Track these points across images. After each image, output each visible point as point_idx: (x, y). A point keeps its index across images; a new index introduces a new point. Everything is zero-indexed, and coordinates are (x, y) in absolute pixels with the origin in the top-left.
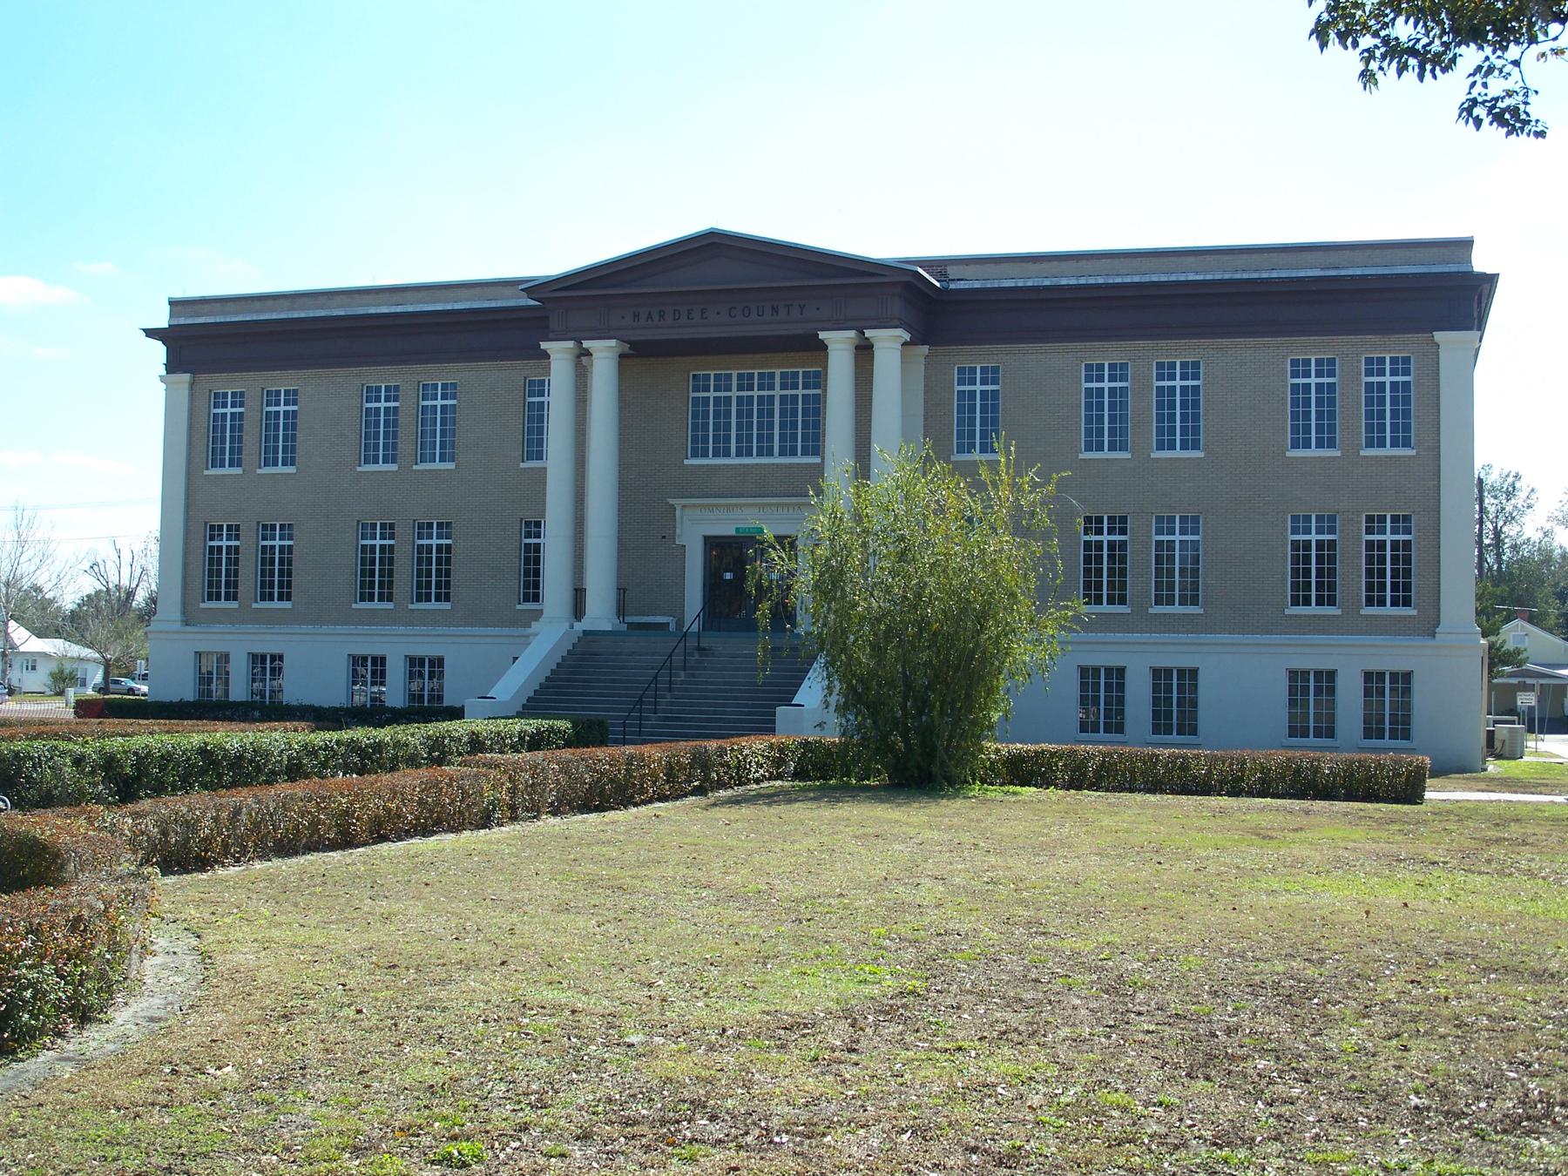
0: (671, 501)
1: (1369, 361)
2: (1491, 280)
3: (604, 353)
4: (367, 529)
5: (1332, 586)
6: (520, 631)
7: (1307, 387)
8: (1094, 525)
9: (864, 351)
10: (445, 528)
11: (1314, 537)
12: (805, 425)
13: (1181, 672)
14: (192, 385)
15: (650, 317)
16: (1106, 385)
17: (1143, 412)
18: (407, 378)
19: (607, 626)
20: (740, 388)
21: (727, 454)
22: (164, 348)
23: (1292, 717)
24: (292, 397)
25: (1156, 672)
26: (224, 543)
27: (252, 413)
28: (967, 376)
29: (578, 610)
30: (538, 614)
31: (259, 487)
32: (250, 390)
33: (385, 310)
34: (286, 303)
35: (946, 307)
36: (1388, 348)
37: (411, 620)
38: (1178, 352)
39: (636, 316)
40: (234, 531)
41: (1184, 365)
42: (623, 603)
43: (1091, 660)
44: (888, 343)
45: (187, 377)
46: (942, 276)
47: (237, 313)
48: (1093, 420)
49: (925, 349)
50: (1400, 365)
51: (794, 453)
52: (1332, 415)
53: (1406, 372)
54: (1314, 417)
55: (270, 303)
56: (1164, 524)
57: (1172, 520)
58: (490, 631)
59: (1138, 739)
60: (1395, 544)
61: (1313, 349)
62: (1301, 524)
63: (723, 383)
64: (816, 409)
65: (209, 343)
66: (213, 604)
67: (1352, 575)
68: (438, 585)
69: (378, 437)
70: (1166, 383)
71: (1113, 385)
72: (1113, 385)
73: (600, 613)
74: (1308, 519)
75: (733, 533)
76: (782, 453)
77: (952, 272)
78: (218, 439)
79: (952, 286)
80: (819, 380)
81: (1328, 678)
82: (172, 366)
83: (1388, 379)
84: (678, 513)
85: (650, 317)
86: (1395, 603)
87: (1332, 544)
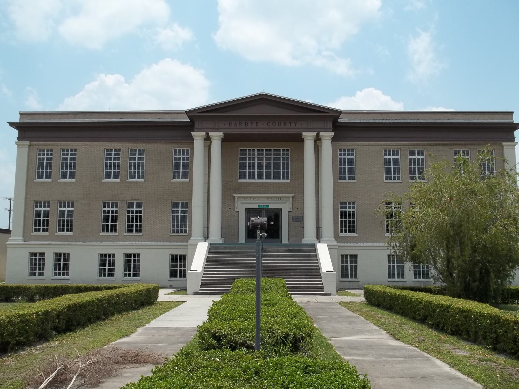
0: (234, 195)
3: (216, 138)
4: (106, 204)
6: (184, 244)
7: (345, 159)
8: (106, 204)
10: (71, 204)
12: (345, 169)
14: (29, 146)
15: (236, 125)
16: (392, 157)
17: (404, 167)
21: (253, 178)
24: (73, 152)
26: (110, 209)
30: (190, 236)
31: (57, 187)
32: (58, 150)
34: (73, 116)
35: (347, 129)
37: (58, 238)
38: (70, 146)
39: (230, 124)
43: (59, 251)
44: (327, 137)
45: (28, 143)
52: (398, 169)
58: (159, 243)
59: (49, 277)
60: (137, 212)
65: (33, 130)
66: (37, 233)
67: (122, 222)
68: (112, 226)
70: (343, 157)
75: (257, 207)
81: (42, 255)
82: (20, 138)
83: (416, 157)
84: (236, 199)
85: (236, 125)
87: (141, 212)
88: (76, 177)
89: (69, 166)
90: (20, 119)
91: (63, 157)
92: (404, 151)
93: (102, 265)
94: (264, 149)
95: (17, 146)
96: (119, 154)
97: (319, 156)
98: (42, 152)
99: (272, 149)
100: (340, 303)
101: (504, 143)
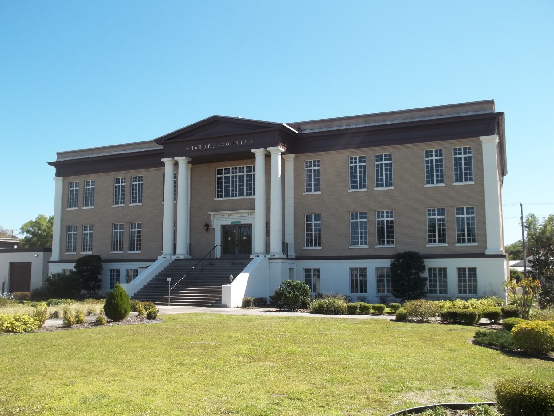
0: (210, 213)
1: (455, 150)
2: (501, 114)
5: (444, 235)
9: (268, 156)
11: (385, 219)
12: (432, 172)
13: (470, 269)
14: (192, 169)
17: (371, 174)
18: (127, 175)
19: (182, 257)
20: (247, 172)
22: (55, 169)
23: (460, 286)
24: (141, 178)
25: (459, 269)
27: (128, 185)
28: (309, 164)
29: (174, 252)
33: (121, 152)
35: (299, 140)
36: (462, 144)
40: (364, 215)
41: (386, 156)
42: (190, 248)
46: (298, 129)
47: (76, 156)
48: (429, 171)
49: (293, 155)
50: (467, 150)
51: (236, 196)
53: (441, 155)
54: (435, 172)
55: (86, 152)
56: (460, 211)
57: (383, 213)
61: (433, 146)
62: (431, 212)
63: (227, 171)
64: (251, 180)
65: (69, 167)
69: (358, 177)
71: (315, 168)
72: (315, 168)
73: (182, 251)
74: (434, 210)
75: (230, 223)
76: (247, 195)
77: (302, 127)
78: (117, 195)
79: (303, 132)
80: (252, 169)
82: (58, 175)
84: (212, 217)
86: (440, 242)
87: (392, 222)
88: (321, 189)
89: (434, 169)
90: (58, 158)
91: (352, 165)
92: (371, 156)
93: (353, 281)
94: (224, 168)
95: (55, 181)
96: (364, 162)
97: (275, 167)
98: (72, 185)
99: (231, 168)
100: (391, 320)
101: (482, 138)
